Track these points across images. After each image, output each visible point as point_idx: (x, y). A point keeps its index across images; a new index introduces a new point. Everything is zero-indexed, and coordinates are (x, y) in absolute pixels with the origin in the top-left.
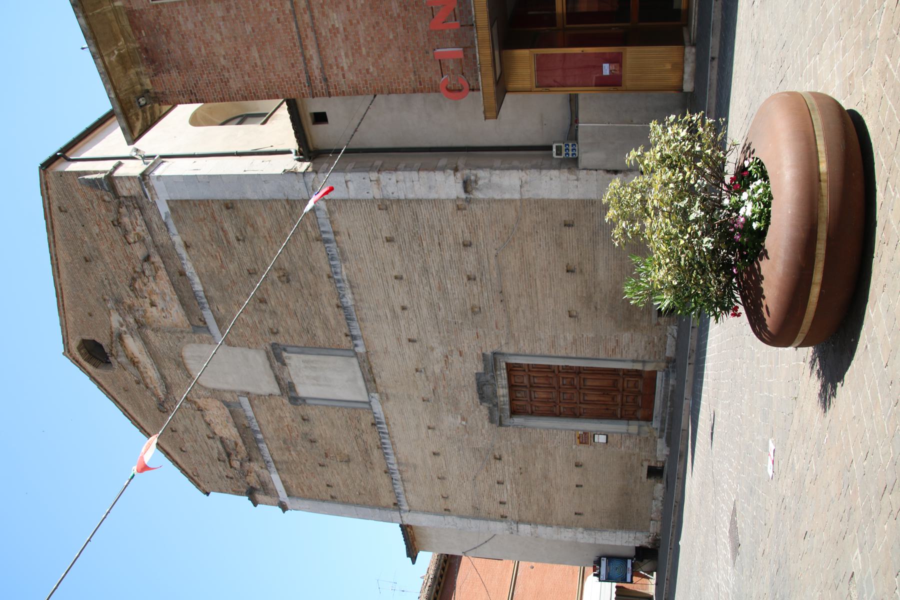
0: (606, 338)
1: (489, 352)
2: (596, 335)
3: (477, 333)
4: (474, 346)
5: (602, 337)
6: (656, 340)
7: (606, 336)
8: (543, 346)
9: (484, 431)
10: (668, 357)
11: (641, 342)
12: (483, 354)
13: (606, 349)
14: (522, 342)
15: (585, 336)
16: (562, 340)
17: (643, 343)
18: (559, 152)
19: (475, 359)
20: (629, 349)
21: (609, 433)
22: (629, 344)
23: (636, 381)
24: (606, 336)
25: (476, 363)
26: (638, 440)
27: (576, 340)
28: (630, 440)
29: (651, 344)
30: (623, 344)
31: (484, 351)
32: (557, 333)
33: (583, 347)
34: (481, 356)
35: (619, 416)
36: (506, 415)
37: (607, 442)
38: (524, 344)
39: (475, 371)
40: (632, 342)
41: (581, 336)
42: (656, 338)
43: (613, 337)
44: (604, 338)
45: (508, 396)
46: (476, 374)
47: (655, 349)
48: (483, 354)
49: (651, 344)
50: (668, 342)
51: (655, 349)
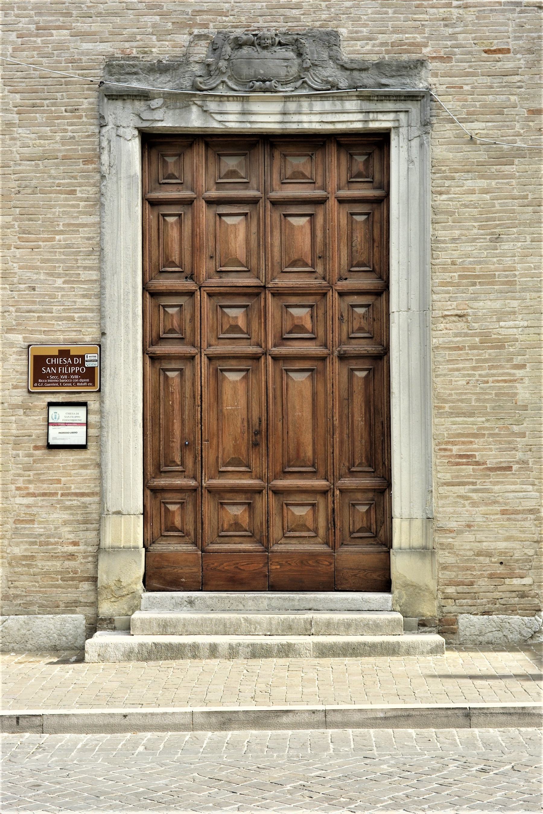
0: (514, 434)
1: (432, 80)
2: (525, 408)
3: (508, 51)
4: (453, 37)
5: (519, 423)
6: (516, 582)
7: (522, 435)
8: (468, 248)
9: (58, 35)
10: (455, 622)
11: (508, 539)
12: (421, 63)
13: (475, 436)
14: (483, 183)
15: (519, 373)
16: (497, 305)
17: (502, 545)
18: (22, 722)
19: (395, 37)
20: (474, 504)
21: (101, 452)
22: (495, 502)
23: (316, 530)
24: (522, 435)
25: (381, 38)
26: (71, 549)
27: (502, 347)
28: (66, 523)
29: (501, 570)
30: (496, 488)
31: (431, 65)
32: (523, 290)
33: (474, 368)
34: (415, 56)
35: (162, 482)
36: (158, 115)
37: (51, 447)
38: (472, 192)
39: (343, 31)
40: (504, 512)
41: (518, 360)
42: (527, 581)
43: (519, 455)
44: (516, 428)
45: (247, 127)
46: (337, 35)
47: (483, 584)
48: (421, 63)
49: (501, 570)
50: (516, 619)
51: (483, 584)
